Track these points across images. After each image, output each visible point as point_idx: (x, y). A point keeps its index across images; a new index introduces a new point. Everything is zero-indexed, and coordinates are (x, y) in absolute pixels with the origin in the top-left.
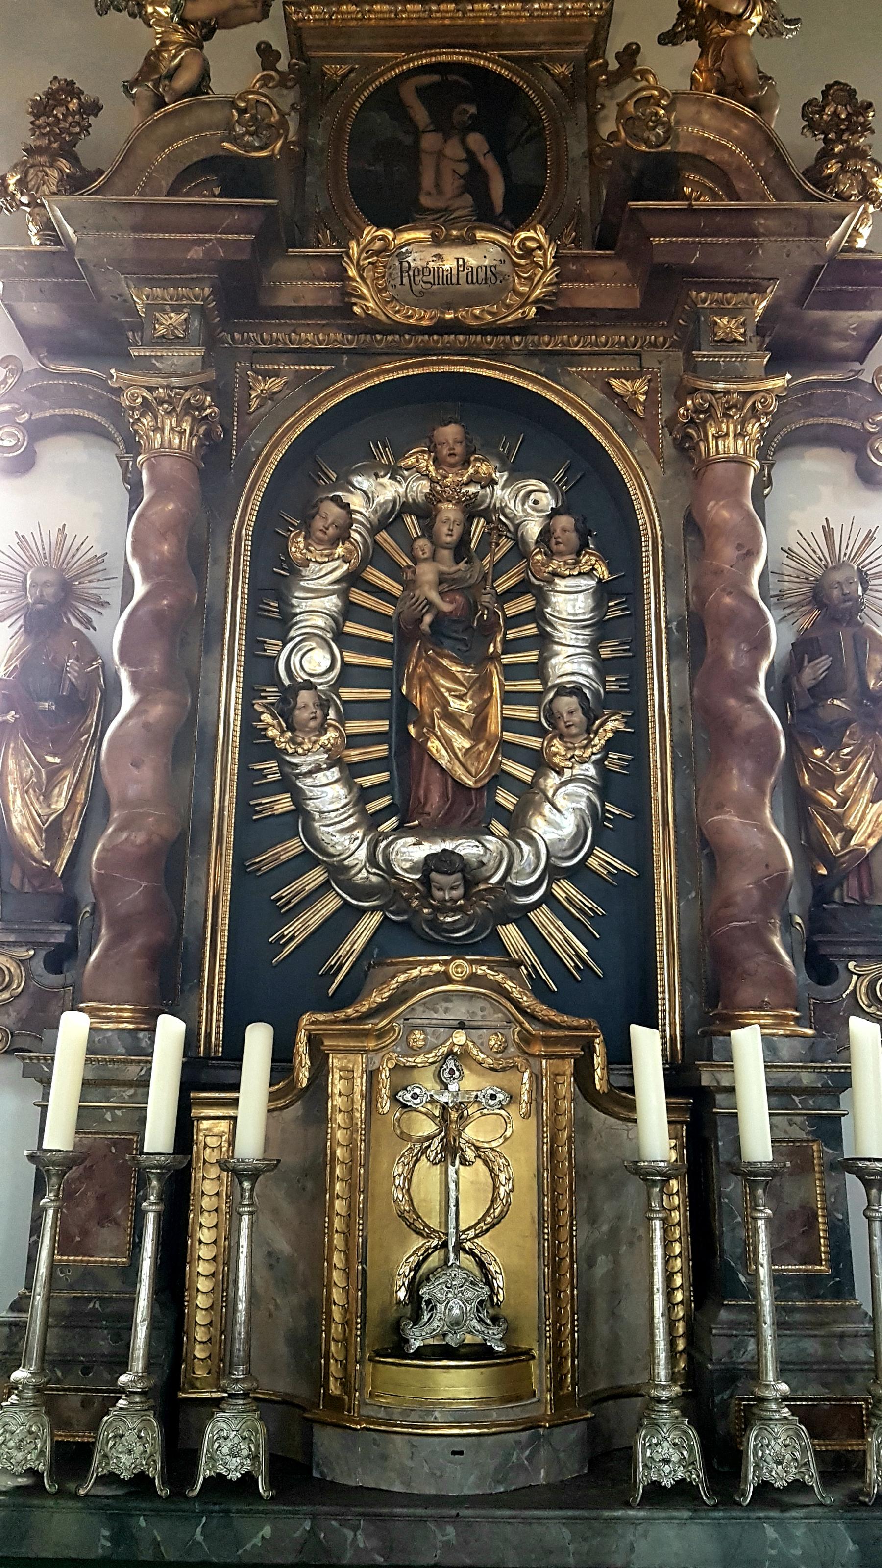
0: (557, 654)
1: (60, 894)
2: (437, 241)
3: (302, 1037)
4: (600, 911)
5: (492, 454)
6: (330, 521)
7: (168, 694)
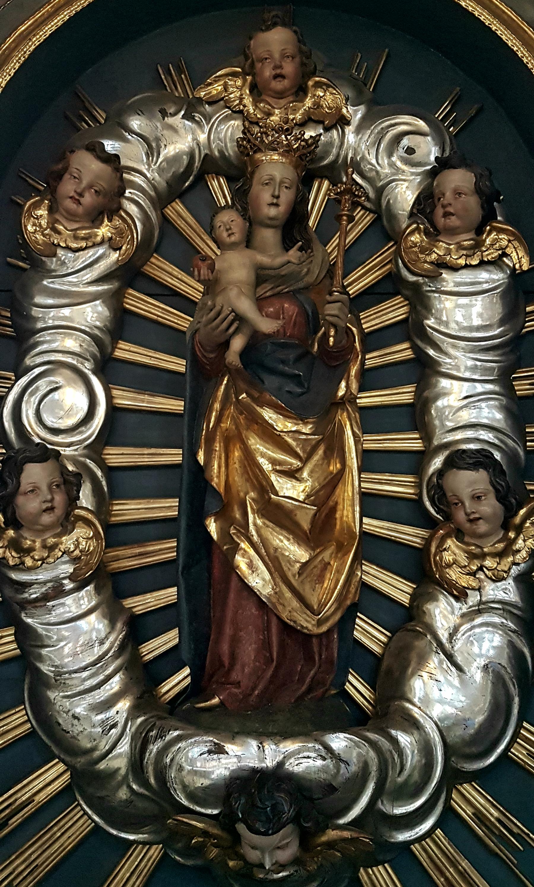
0: (445, 394)
6: (85, 183)
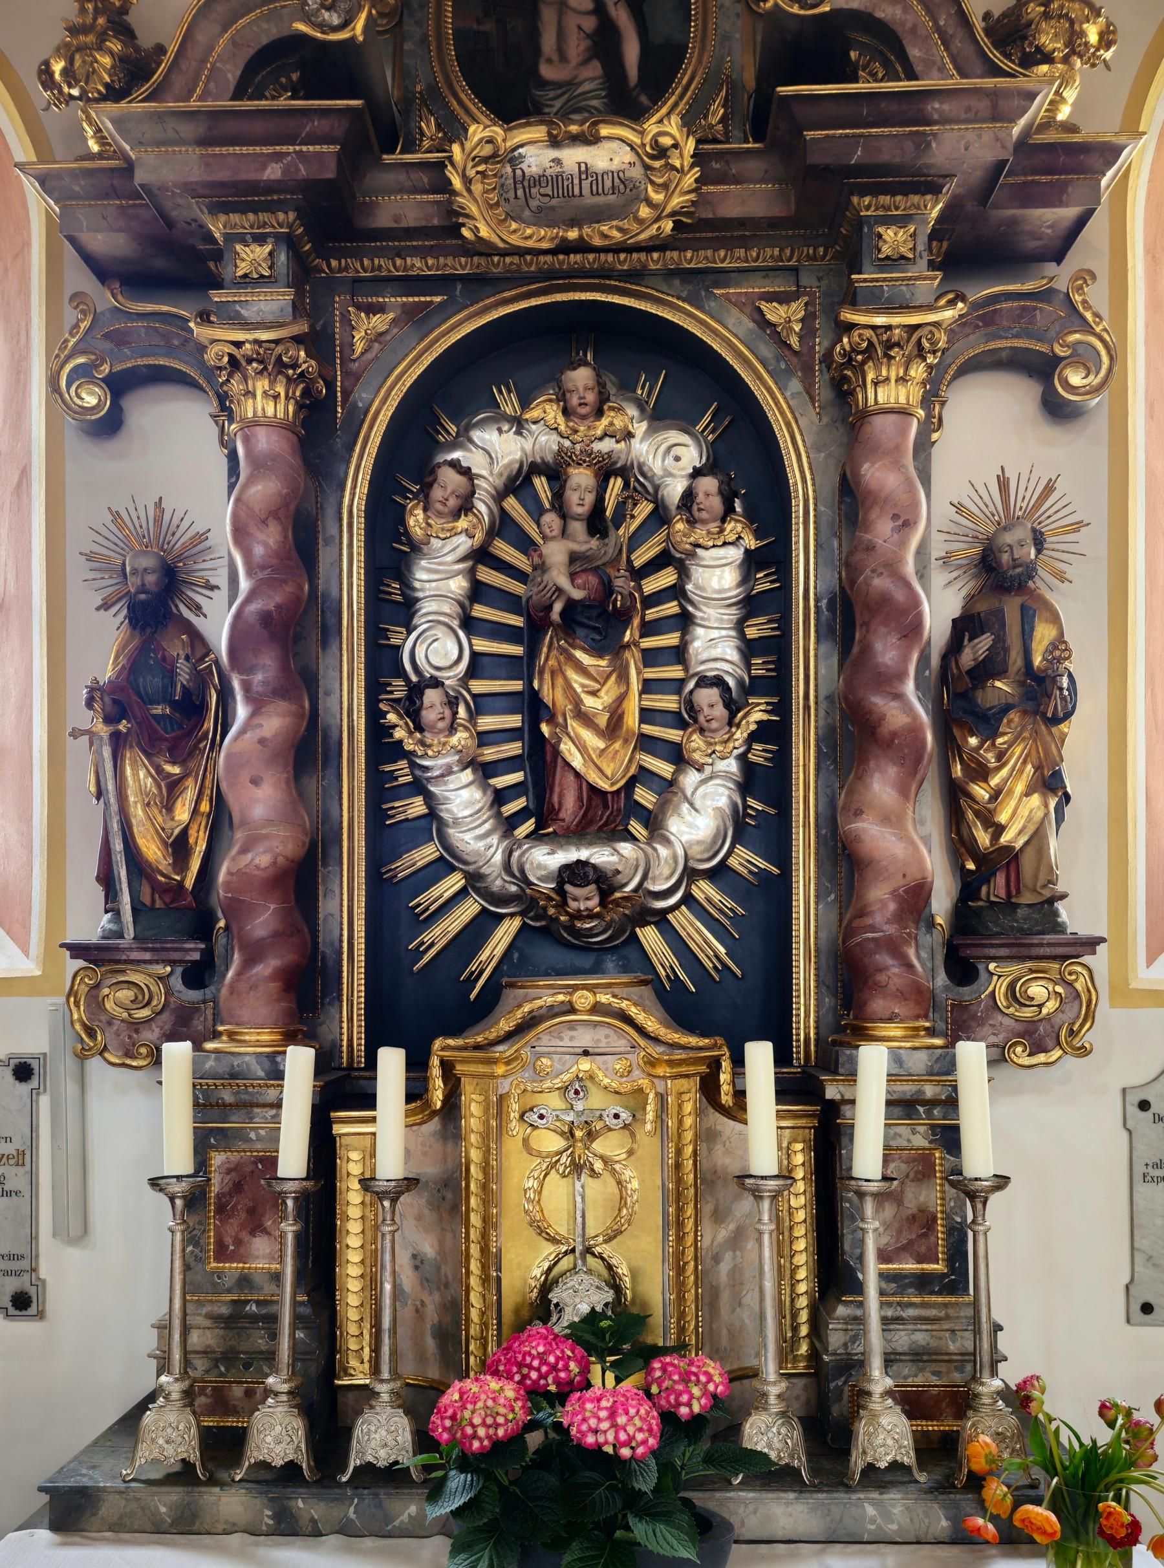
1: (193, 910)
2: (555, 142)
3: (435, 1061)
4: (740, 911)
5: (629, 400)
6: (449, 490)
7: (283, 705)
